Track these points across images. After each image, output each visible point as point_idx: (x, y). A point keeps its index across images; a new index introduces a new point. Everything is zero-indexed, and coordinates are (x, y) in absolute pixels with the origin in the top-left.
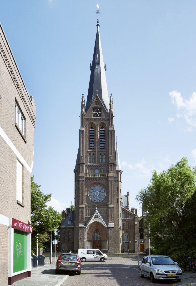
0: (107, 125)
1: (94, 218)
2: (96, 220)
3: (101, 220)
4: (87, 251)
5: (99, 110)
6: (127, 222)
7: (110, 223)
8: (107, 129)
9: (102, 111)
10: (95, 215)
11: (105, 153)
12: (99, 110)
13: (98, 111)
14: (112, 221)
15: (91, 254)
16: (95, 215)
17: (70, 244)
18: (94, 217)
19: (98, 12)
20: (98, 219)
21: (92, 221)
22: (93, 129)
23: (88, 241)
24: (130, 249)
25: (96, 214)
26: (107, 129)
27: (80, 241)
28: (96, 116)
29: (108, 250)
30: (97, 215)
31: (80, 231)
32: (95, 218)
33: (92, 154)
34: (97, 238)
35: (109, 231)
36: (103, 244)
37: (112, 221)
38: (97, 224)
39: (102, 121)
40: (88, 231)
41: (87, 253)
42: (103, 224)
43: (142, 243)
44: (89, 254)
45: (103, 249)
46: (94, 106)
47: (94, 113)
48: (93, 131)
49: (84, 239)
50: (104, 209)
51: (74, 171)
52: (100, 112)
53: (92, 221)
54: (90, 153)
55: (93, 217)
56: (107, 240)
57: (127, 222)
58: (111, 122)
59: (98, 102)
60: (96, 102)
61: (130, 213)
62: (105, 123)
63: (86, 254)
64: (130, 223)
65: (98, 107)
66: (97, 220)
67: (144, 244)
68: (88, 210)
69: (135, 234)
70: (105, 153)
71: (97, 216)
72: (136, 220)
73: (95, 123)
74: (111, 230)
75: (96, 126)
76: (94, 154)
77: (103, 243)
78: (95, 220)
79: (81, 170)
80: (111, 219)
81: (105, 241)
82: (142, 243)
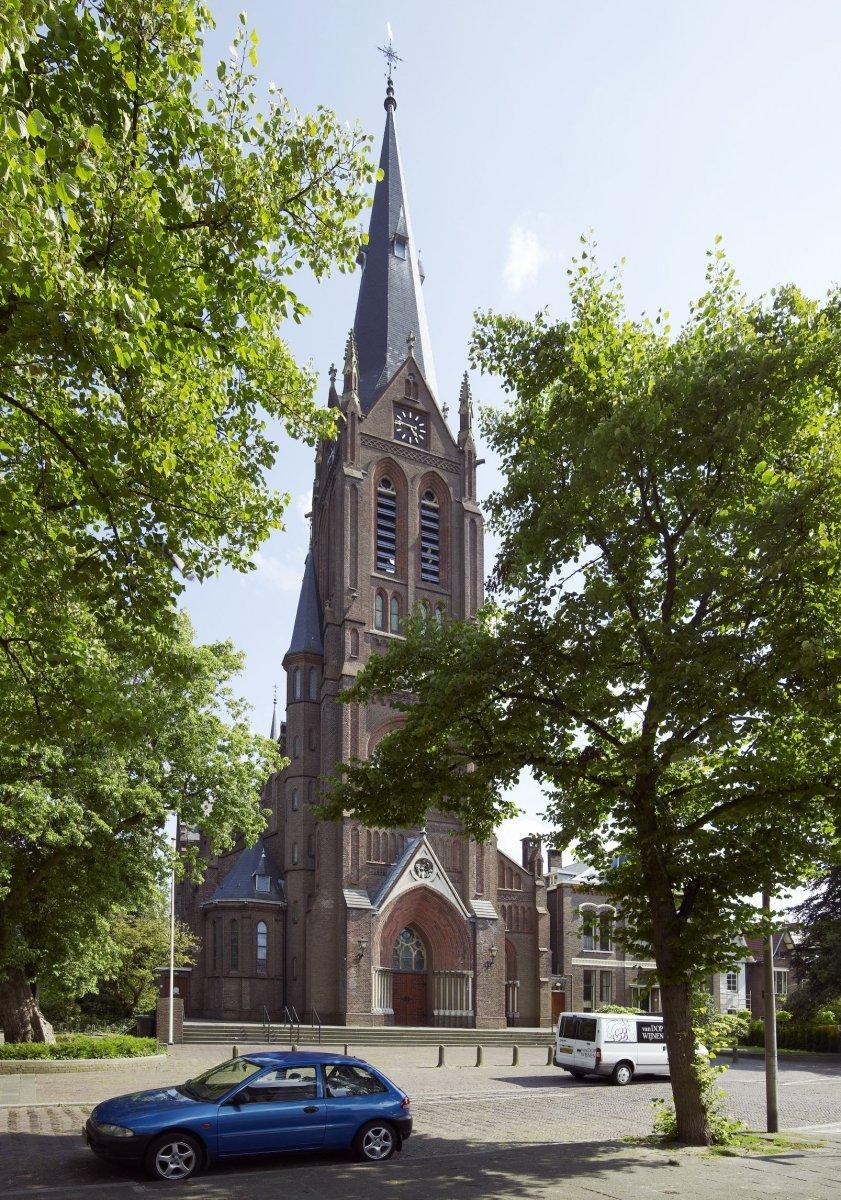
0: (451, 489)
1: (413, 873)
2: (422, 881)
3: (441, 885)
4: (640, 1026)
5: (420, 421)
6: (506, 905)
7: (477, 897)
8: (455, 506)
9: (432, 426)
10: (418, 857)
11: (445, 600)
12: (420, 421)
13: (416, 424)
14: (482, 891)
15: (655, 1041)
16: (418, 857)
17: (266, 982)
18: (415, 868)
19: (390, 54)
20: (433, 876)
21: (405, 884)
22: (394, 493)
23: (382, 973)
24: (316, 1005)
25: (423, 856)
26: (455, 506)
27: (352, 972)
28: (404, 441)
29: (471, 1014)
30: (427, 861)
31: (352, 925)
32: (417, 872)
33: (390, 593)
34: (407, 962)
35: (480, 934)
36: (443, 988)
37: (482, 891)
38: (424, 898)
39: (431, 469)
40: (385, 926)
41: (641, 1039)
42: (453, 901)
43: (557, 988)
44: (647, 1041)
45: (445, 1008)
46: (399, 396)
47: (400, 423)
48: (392, 498)
49: (370, 962)
50: (445, 839)
51: (288, 662)
52: (422, 428)
53: (405, 884)
54: (382, 584)
55: (411, 867)
56: (471, 973)
57: (506, 905)
58: (470, 483)
59: (415, 384)
60: (408, 381)
61: (515, 870)
62: (446, 481)
63: (635, 1040)
64: (517, 908)
65: (417, 406)
66: (427, 882)
67: (563, 994)
68: (376, 832)
69: (537, 954)
70: (445, 600)
71: (426, 865)
72: (538, 899)
73: (408, 467)
74: (485, 928)
75: (409, 480)
76: (396, 596)
77: (439, 983)
78: (420, 882)
79: (349, 649)
80: (480, 882)
81: (452, 975)
82: (557, 988)
